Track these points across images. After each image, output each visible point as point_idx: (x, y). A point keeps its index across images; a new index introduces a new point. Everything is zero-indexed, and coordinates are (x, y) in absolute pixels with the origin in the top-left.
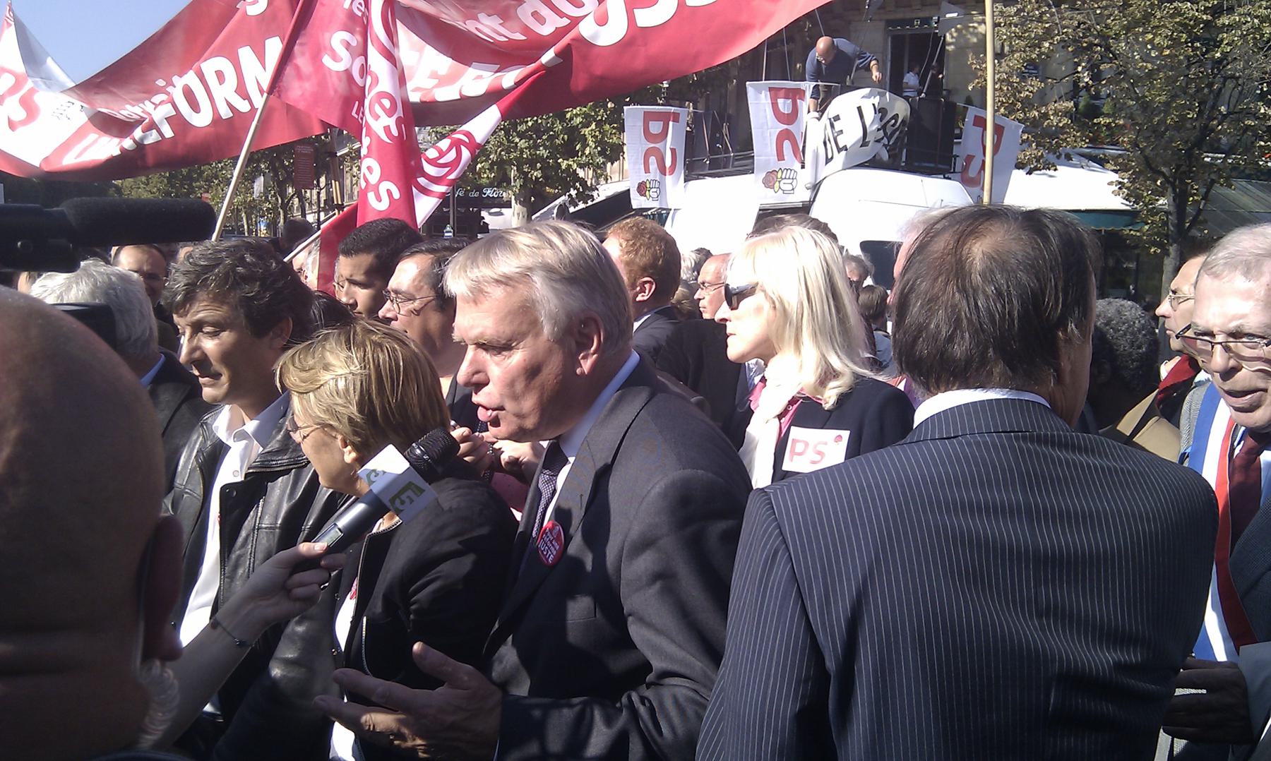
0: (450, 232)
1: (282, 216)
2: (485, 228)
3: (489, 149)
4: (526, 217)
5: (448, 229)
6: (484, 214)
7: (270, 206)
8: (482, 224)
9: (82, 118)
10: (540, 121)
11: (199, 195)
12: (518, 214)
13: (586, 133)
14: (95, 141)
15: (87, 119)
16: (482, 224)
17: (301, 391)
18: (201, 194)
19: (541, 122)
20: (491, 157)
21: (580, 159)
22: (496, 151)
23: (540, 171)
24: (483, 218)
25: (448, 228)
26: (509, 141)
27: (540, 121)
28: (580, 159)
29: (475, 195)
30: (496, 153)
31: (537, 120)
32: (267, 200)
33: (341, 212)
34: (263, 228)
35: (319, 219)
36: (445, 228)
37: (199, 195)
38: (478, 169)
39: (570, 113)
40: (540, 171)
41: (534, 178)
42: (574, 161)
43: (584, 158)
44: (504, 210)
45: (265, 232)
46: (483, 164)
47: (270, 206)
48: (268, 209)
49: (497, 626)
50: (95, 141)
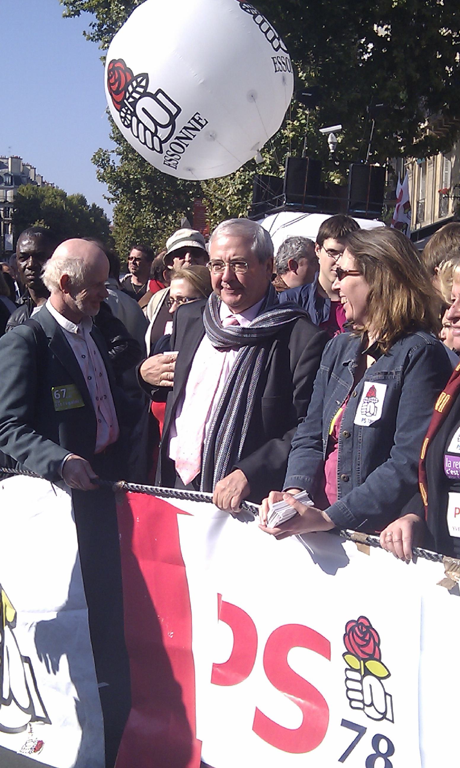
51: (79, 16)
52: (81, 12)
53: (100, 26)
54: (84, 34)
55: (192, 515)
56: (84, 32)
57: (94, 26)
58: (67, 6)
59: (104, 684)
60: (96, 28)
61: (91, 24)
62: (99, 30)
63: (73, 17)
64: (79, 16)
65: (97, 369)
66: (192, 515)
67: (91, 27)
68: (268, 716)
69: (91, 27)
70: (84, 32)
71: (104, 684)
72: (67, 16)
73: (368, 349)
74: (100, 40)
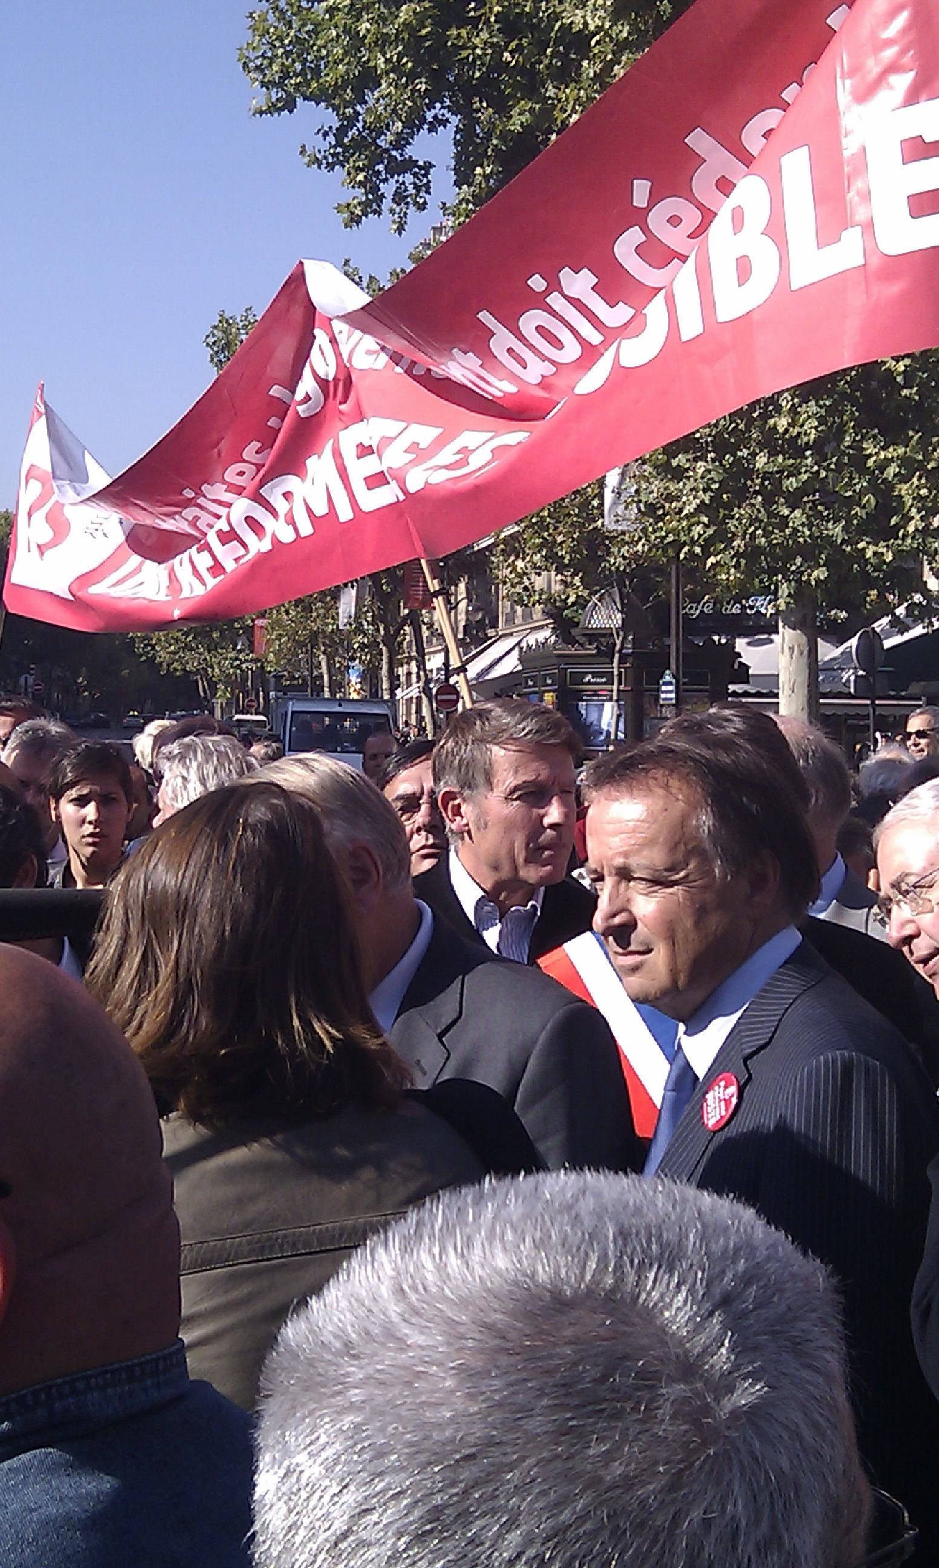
0: (670, 684)
1: (385, 658)
2: (742, 674)
3: (733, 529)
4: (806, 653)
5: (667, 678)
6: (740, 644)
7: (366, 641)
8: (736, 666)
9: (118, 537)
10: (823, 474)
11: (249, 622)
12: (791, 649)
13: (903, 493)
14: (138, 570)
15: (122, 538)
16: (736, 666)
17: (447, 462)
18: (253, 621)
19: (827, 476)
20: (735, 544)
21: (900, 542)
22: (745, 533)
23: (825, 568)
24: (739, 655)
25: (667, 678)
26: (770, 514)
27: (823, 474)
28: (900, 542)
29: (734, 611)
30: (744, 539)
31: (818, 472)
32: (360, 630)
33: (399, 804)
34: (354, 679)
35: (446, 664)
36: (662, 677)
37: (249, 622)
38: (708, 564)
39: (874, 458)
40: (825, 568)
41: (813, 583)
42: (887, 546)
43: (909, 541)
44: (774, 637)
45: (359, 686)
46: (718, 558)
47: (366, 641)
48: (363, 646)
49: (906, 1515)
50: (138, 570)
51: (291, 111)
52: (299, 101)
53: (341, 132)
54: (301, 152)
55: (328, 489)
56: (303, 147)
57: (326, 134)
58: (268, 89)
59: (891, 804)
60: (331, 139)
61: (319, 130)
62: (339, 143)
63: (276, 115)
64: (291, 111)
65: (223, 454)
66: (328, 489)
67: (320, 134)
68: (615, 1034)
69: (320, 134)
70: (303, 147)
71: (891, 804)
72: (261, 113)
73: (858, 635)
74: (337, 167)
